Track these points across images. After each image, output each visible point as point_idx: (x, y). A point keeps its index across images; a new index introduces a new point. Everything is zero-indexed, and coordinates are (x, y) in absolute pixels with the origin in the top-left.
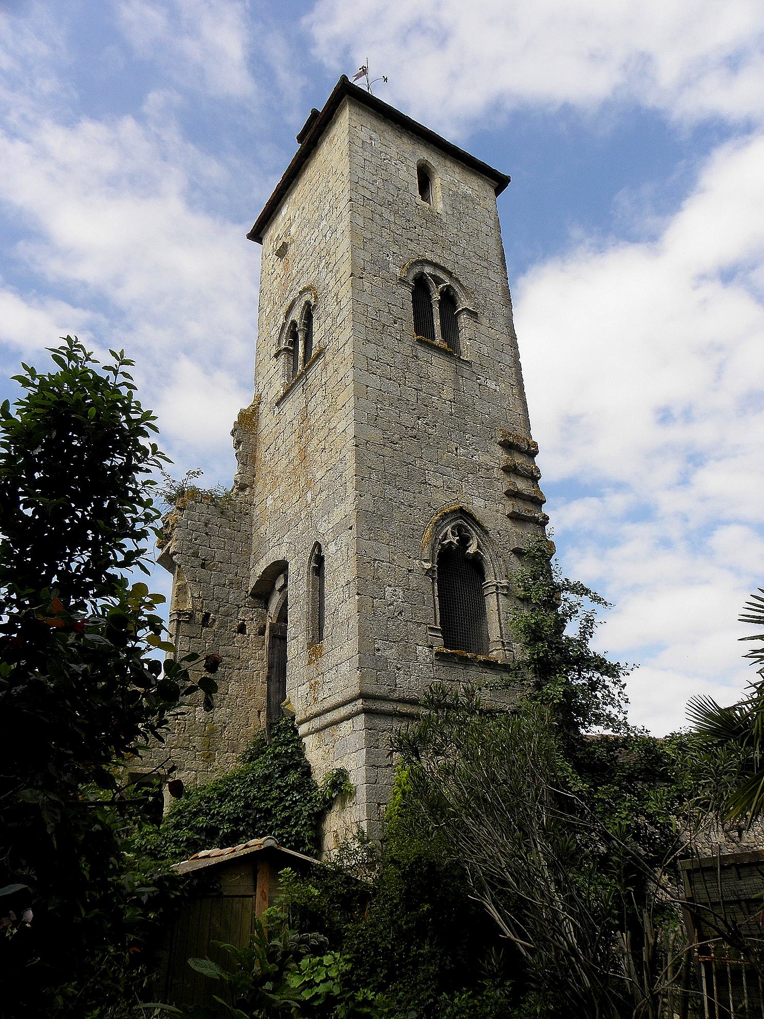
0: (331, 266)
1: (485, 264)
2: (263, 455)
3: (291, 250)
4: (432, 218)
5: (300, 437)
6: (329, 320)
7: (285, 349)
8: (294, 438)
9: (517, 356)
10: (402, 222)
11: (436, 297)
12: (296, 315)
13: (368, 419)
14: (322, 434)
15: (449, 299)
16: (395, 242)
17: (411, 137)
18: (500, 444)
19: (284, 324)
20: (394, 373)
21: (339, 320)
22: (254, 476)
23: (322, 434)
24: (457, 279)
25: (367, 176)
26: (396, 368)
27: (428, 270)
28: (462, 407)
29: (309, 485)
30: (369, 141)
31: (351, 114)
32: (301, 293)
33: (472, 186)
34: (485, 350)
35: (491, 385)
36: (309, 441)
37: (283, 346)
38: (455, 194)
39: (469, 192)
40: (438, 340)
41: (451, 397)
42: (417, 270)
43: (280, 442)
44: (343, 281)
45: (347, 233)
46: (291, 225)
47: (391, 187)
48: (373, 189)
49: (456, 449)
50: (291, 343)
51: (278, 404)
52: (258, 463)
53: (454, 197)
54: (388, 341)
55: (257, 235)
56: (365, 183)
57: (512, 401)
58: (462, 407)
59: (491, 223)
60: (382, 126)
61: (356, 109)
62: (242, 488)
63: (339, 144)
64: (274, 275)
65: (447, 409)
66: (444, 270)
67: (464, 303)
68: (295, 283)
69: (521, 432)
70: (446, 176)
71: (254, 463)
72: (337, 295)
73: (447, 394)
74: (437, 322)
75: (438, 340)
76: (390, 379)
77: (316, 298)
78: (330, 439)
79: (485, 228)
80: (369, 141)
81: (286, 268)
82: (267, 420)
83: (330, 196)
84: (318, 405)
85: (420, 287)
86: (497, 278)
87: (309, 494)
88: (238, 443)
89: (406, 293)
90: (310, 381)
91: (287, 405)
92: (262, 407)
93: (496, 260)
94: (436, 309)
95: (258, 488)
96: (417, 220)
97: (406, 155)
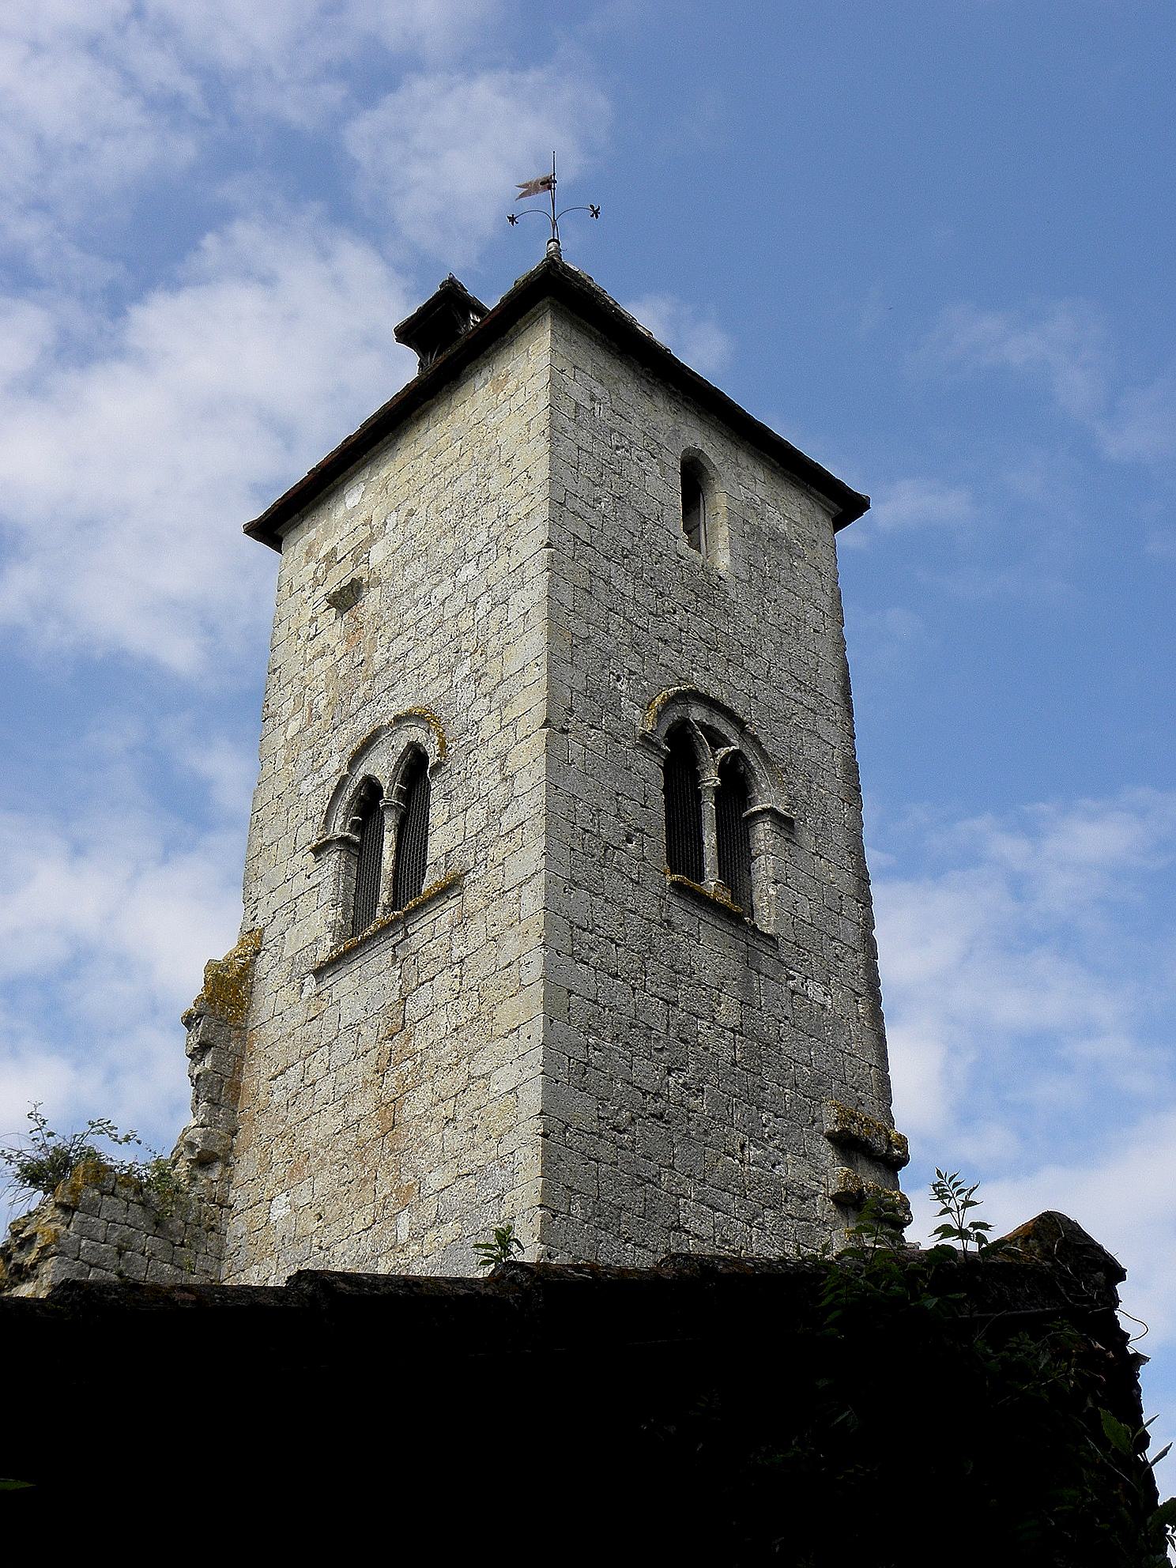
0: (487, 684)
1: (810, 700)
2: (257, 1077)
3: (372, 600)
4: (707, 589)
5: (381, 1072)
6: (478, 813)
7: (343, 840)
8: (363, 1068)
9: (868, 923)
10: (646, 597)
11: (711, 778)
12: (382, 766)
13: (569, 1070)
14: (447, 1083)
15: (736, 783)
16: (635, 645)
17: (671, 396)
18: (831, 1137)
19: (343, 780)
20: (618, 957)
21: (508, 821)
22: (234, 1133)
23: (447, 1083)
24: (755, 738)
25: (583, 487)
26: (629, 949)
27: (697, 714)
28: (759, 1047)
29: (407, 1196)
30: (587, 404)
31: (555, 340)
32: (398, 719)
33: (789, 512)
34: (806, 910)
35: (815, 991)
36: (405, 1089)
37: (340, 833)
38: (756, 532)
39: (783, 527)
40: (711, 883)
41: (734, 1020)
42: (674, 715)
43: (317, 1068)
44: (522, 731)
45: (539, 617)
46: (371, 540)
47: (630, 514)
48: (594, 520)
49: (743, 1147)
50: (356, 827)
51: (319, 973)
52: (245, 1102)
53: (755, 538)
54: (614, 883)
55: (272, 529)
56: (577, 505)
57: (856, 1032)
58: (759, 1047)
59: (825, 601)
60: (614, 370)
61: (565, 329)
62: (204, 1161)
63: (520, 399)
64: (318, 644)
65: (726, 1049)
66: (729, 714)
67: (766, 796)
68: (379, 686)
69: (870, 1110)
70: (739, 487)
71: (235, 1099)
72: (503, 757)
73: (728, 1012)
74: (710, 839)
75: (711, 883)
76: (616, 976)
77: (443, 746)
78: (472, 1100)
79: (812, 615)
80: (587, 404)
81: (352, 637)
82: (278, 1004)
83: (490, 513)
84: (438, 1008)
85: (679, 751)
86: (832, 733)
87: (404, 1220)
88: (197, 1053)
89: (650, 769)
90: (415, 942)
91: (344, 983)
92: (264, 963)
93: (835, 695)
94: (709, 807)
95: (246, 1166)
96: (679, 595)
97: (662, 439)
